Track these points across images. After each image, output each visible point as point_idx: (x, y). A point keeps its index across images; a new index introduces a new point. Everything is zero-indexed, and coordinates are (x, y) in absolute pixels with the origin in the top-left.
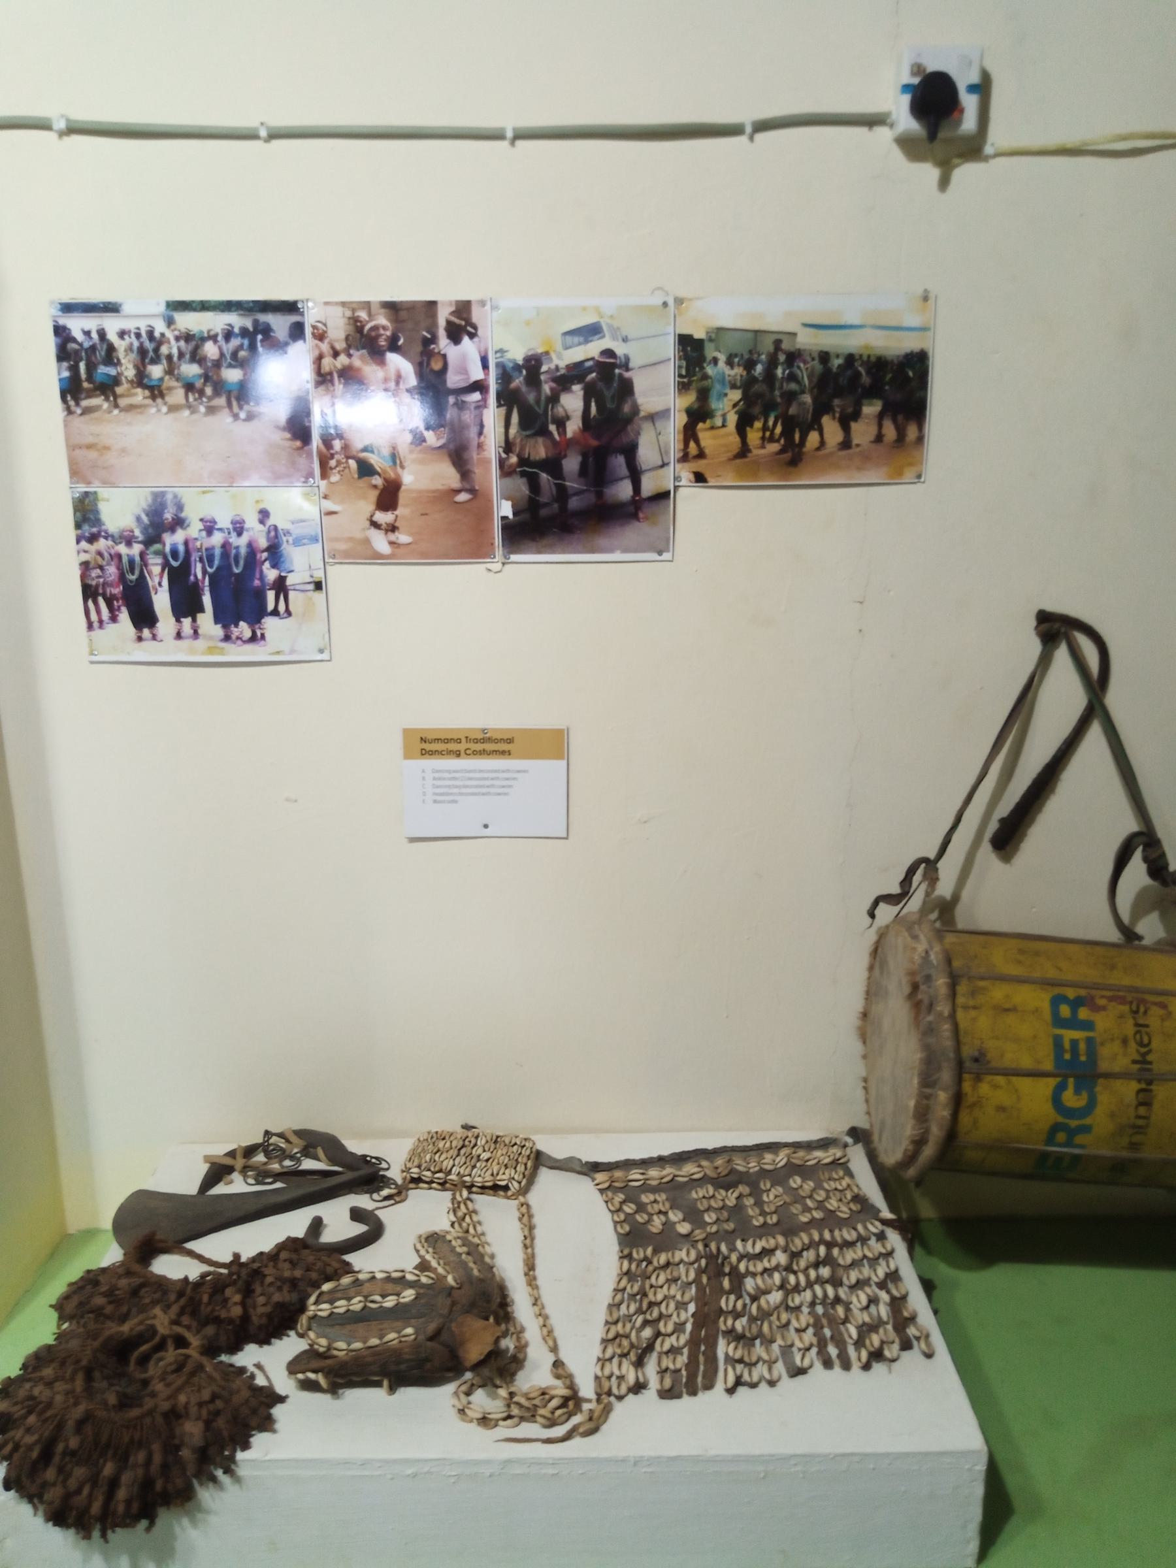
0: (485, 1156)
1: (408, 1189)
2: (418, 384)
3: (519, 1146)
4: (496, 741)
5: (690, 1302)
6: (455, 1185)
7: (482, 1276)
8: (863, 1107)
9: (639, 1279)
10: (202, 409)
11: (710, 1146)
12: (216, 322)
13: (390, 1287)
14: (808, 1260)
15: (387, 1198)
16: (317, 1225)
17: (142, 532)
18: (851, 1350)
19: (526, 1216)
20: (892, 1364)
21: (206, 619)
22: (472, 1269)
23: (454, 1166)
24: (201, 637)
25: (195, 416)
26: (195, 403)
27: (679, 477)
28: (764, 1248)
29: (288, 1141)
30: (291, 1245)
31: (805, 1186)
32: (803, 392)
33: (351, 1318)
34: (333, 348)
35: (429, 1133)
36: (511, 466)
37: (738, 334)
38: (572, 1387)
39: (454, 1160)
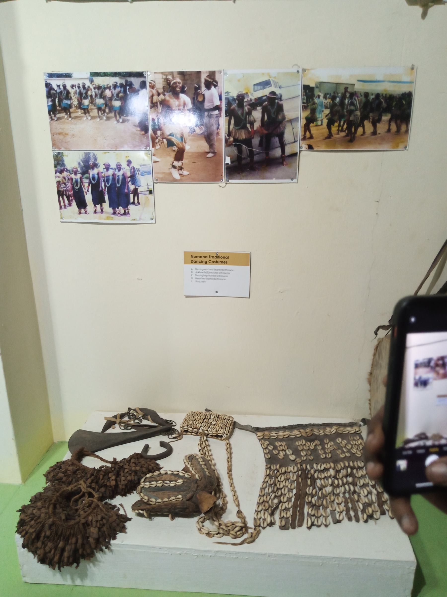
0: (213, 423)
1: (183, 435)
2: (192, 107)
3: (227, 419)
4: (222, 257)
5: (294, 489)
6: (201, 434)
7: (210, 475)
8: (369, 411)
9: (273, 477)
10: (105, 118)
11: (304, 423)
12: (110, 81)
13: (173, 478)
14: (343, 474)
15: (174, 438)
16: (147, 448)
17: (80, 169)
18: (360, 514)
19: (229, 448)
20: (377, 521)
21: (106, 206)
22: (206, 472)
23: (201, 426)
24: (104, 213)
25: (101, 121)
26: (102, 115)
27: (302, 147)
28: (325, 468)
29: (137, 412)
30: (136, 456)
31: (343, 442)
32: (356, 110)
33: (157, 489)
34: (158, 92)
35: (192, 412)
36: (230, 142)
37: (329, 85)
38: (245, 523)
39: (201, 424)
